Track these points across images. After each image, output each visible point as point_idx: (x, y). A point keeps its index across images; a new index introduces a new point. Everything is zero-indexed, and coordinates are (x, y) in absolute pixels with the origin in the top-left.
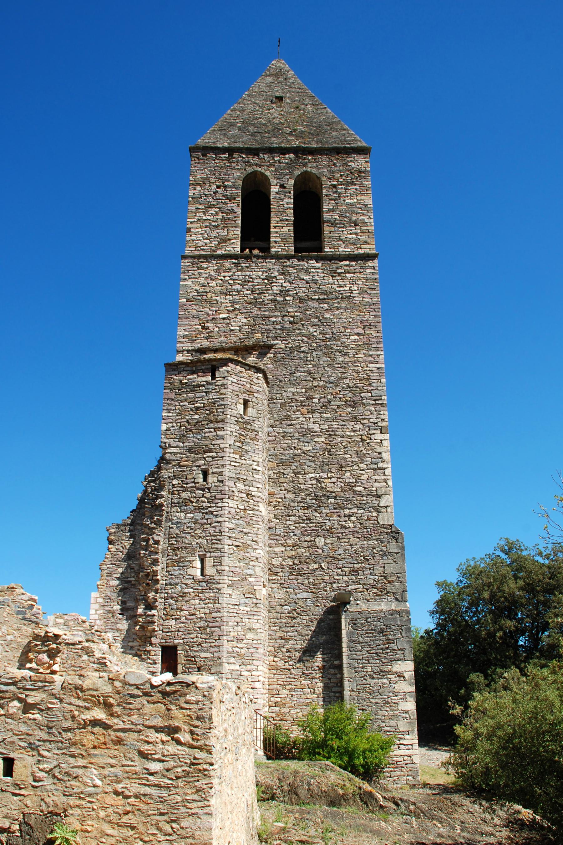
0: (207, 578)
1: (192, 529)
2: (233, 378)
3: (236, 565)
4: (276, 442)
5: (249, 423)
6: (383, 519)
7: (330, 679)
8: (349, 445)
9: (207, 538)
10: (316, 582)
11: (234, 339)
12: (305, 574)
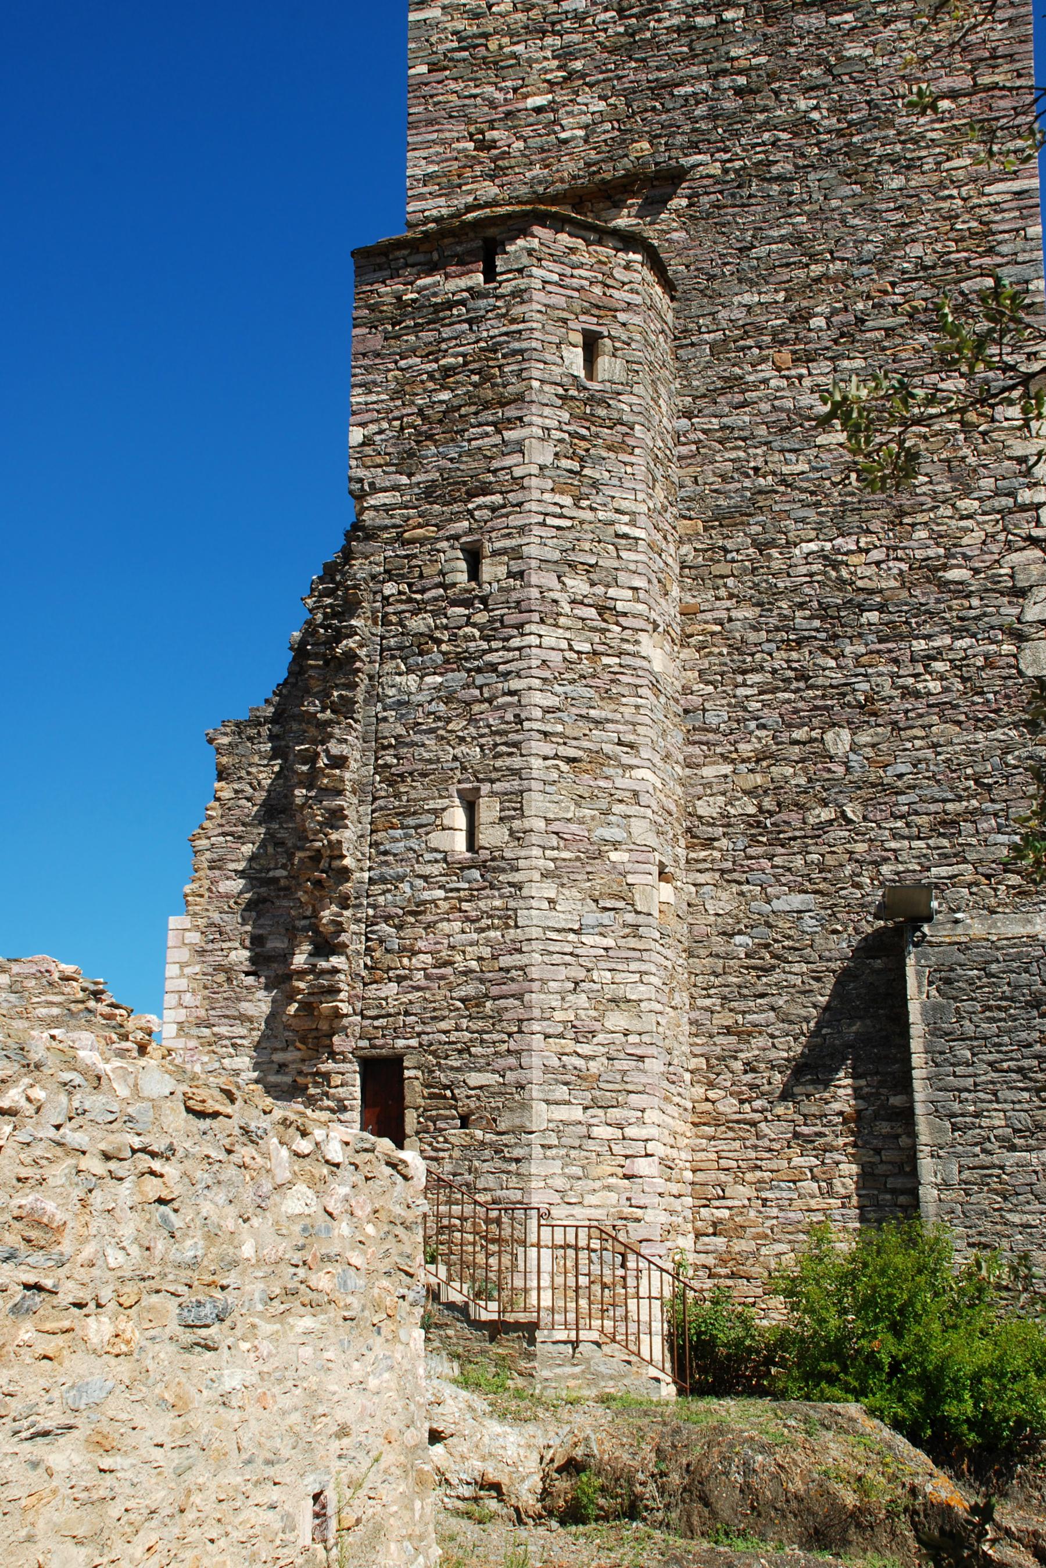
0: (484, 854)
1: (439, 719)
2: (549, 268)
3: (570, 815)
4: (699, 458)
5: (603, 402)
7: (878, 1152)
8: (923, 446)
9: (483, 741)
10: (830, 860)
11: (569, 167)
12: (794, 838)
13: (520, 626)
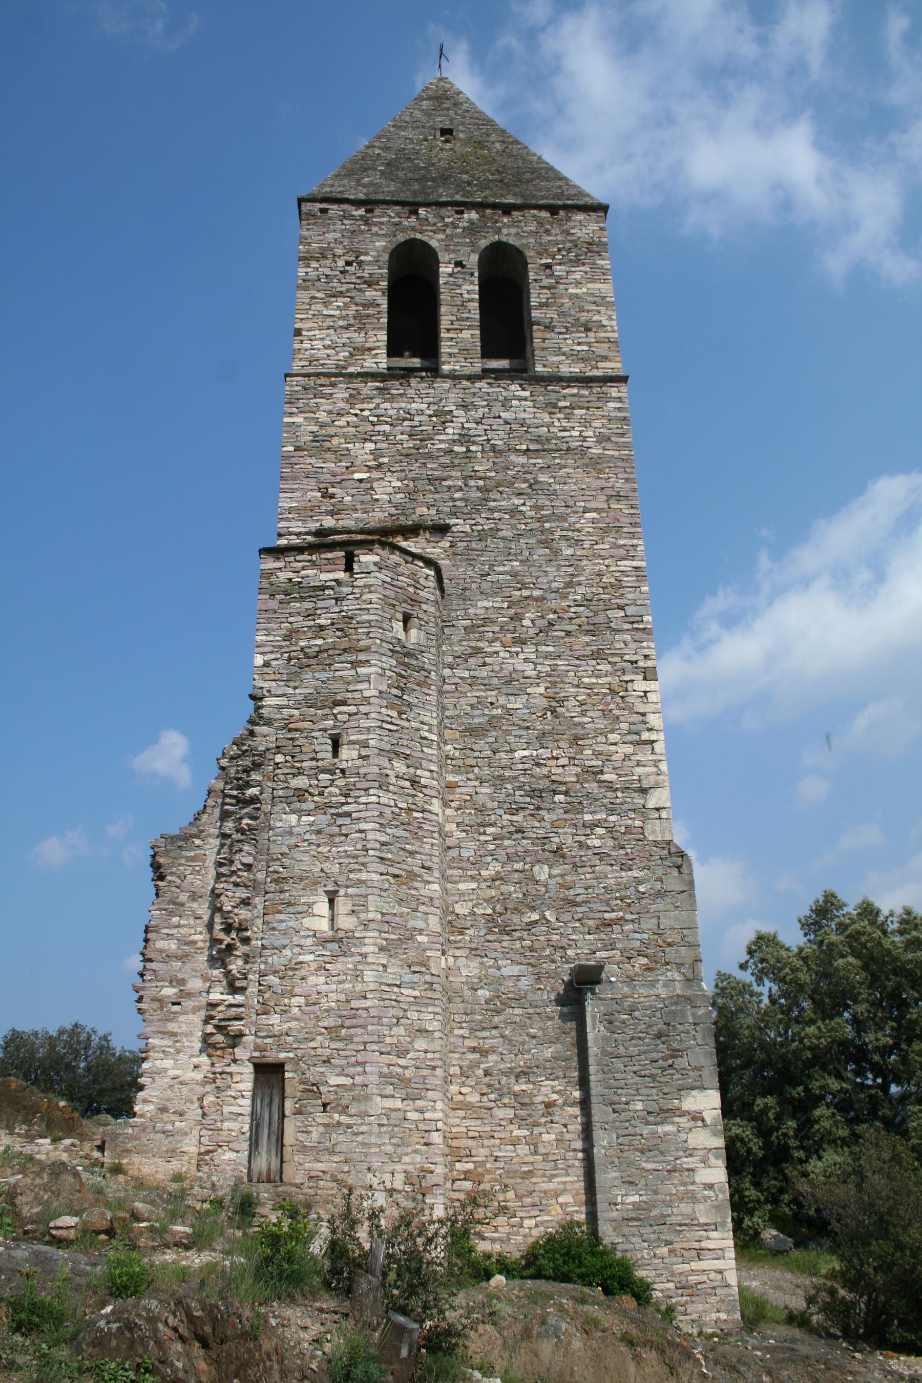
0: (341, 934)
6: (654, 832)
10: (537, 945)
13: (366, 790)
